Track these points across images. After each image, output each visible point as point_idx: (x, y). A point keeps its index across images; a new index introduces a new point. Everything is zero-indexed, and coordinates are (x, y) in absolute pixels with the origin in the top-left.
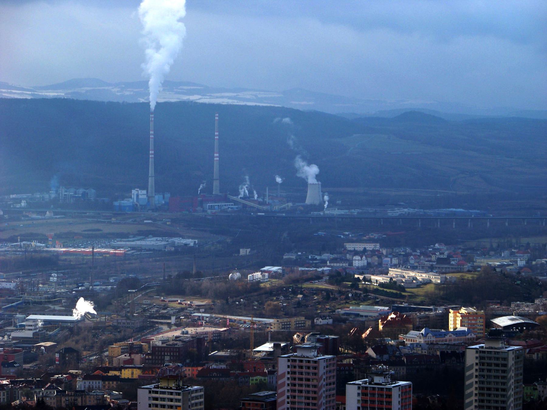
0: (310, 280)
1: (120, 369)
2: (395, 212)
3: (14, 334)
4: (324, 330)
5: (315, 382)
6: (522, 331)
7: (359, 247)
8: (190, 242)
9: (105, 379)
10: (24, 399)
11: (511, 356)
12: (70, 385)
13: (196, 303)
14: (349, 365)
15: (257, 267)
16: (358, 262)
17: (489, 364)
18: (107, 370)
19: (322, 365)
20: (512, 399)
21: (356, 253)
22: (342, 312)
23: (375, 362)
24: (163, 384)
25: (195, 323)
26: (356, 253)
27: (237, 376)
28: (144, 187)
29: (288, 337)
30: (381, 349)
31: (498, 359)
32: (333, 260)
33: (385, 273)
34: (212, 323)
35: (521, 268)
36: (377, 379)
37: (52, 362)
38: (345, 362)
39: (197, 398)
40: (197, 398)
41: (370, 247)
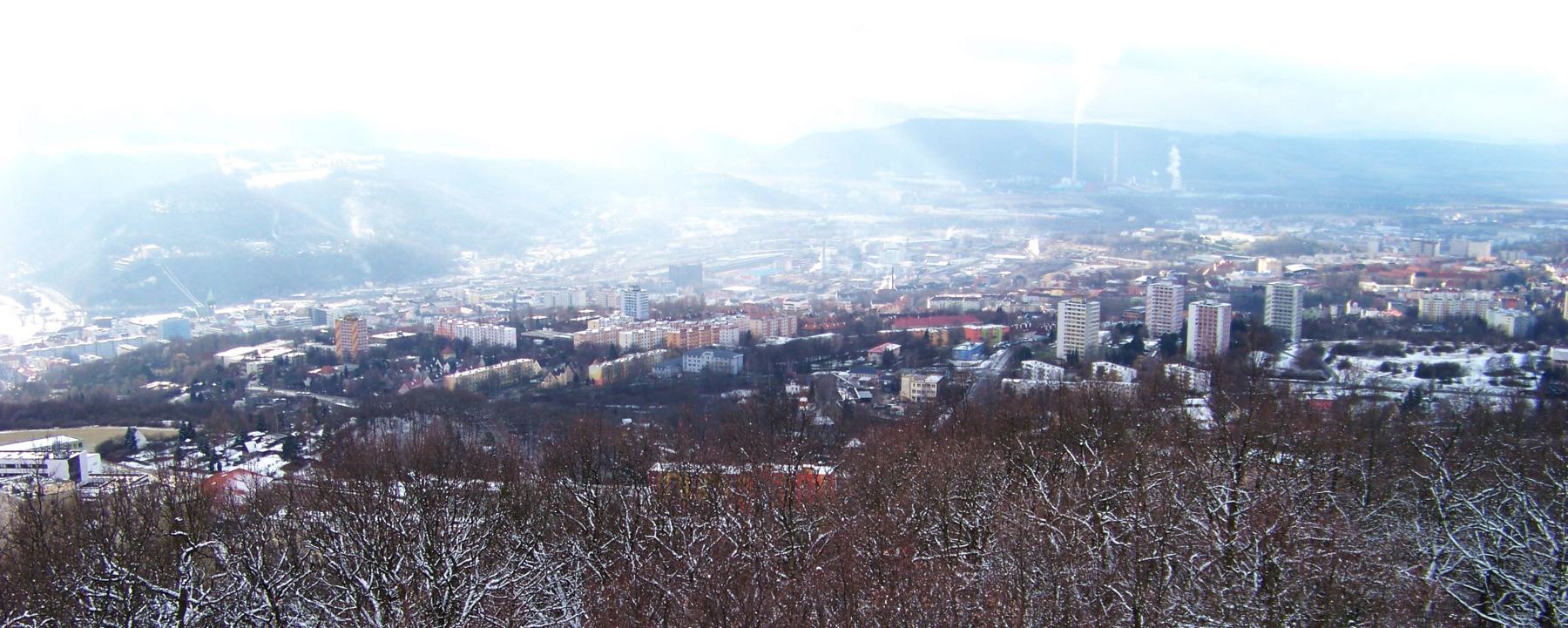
0: (1172, 237)
1: (1050, 289)
2: (1229, 196)
3: (986, 266)
4: (1179, 269)
5: (1170, 302)
6: (1305, 274)
7: (1204, 217)
8: (1098, 212)
9: (1040, 295)
10: (990, 307)
11: (1296, 291)
12: (1019, 299)
13: (1100, 249)
14: (1194, 292)
15: (1140, 228)
16: (1203, 227)
17: (1281, 295)
18: (1043, 290)
19: (1175, 291)
20: (1295, 318)
21: (1201, 221)
22: (1191, 258)
23: (1210, 290)
24: (1074, 300)
25: (1098, 262)
26: (1201, 221)
27: (1124, 296)
28: (1069, 176)
29: (1156, 273)
30: (1214, 282)
31: (1286, 291)
32: (1187, 226)
33: (1219, 234)
34: (1109, 262)
35: (1307, 234)
36: (1209, 301)
37: (1008, 284)
38: (1191, 290)
39: (1095, 309)
40: (1095, 309)
41: (1211, 217)
